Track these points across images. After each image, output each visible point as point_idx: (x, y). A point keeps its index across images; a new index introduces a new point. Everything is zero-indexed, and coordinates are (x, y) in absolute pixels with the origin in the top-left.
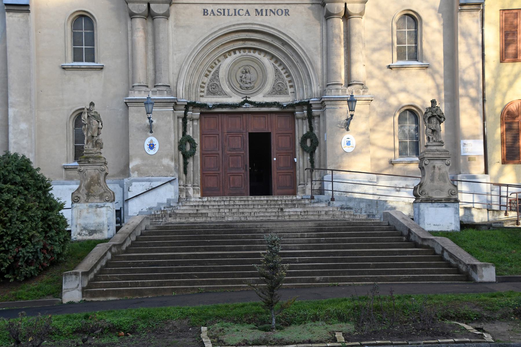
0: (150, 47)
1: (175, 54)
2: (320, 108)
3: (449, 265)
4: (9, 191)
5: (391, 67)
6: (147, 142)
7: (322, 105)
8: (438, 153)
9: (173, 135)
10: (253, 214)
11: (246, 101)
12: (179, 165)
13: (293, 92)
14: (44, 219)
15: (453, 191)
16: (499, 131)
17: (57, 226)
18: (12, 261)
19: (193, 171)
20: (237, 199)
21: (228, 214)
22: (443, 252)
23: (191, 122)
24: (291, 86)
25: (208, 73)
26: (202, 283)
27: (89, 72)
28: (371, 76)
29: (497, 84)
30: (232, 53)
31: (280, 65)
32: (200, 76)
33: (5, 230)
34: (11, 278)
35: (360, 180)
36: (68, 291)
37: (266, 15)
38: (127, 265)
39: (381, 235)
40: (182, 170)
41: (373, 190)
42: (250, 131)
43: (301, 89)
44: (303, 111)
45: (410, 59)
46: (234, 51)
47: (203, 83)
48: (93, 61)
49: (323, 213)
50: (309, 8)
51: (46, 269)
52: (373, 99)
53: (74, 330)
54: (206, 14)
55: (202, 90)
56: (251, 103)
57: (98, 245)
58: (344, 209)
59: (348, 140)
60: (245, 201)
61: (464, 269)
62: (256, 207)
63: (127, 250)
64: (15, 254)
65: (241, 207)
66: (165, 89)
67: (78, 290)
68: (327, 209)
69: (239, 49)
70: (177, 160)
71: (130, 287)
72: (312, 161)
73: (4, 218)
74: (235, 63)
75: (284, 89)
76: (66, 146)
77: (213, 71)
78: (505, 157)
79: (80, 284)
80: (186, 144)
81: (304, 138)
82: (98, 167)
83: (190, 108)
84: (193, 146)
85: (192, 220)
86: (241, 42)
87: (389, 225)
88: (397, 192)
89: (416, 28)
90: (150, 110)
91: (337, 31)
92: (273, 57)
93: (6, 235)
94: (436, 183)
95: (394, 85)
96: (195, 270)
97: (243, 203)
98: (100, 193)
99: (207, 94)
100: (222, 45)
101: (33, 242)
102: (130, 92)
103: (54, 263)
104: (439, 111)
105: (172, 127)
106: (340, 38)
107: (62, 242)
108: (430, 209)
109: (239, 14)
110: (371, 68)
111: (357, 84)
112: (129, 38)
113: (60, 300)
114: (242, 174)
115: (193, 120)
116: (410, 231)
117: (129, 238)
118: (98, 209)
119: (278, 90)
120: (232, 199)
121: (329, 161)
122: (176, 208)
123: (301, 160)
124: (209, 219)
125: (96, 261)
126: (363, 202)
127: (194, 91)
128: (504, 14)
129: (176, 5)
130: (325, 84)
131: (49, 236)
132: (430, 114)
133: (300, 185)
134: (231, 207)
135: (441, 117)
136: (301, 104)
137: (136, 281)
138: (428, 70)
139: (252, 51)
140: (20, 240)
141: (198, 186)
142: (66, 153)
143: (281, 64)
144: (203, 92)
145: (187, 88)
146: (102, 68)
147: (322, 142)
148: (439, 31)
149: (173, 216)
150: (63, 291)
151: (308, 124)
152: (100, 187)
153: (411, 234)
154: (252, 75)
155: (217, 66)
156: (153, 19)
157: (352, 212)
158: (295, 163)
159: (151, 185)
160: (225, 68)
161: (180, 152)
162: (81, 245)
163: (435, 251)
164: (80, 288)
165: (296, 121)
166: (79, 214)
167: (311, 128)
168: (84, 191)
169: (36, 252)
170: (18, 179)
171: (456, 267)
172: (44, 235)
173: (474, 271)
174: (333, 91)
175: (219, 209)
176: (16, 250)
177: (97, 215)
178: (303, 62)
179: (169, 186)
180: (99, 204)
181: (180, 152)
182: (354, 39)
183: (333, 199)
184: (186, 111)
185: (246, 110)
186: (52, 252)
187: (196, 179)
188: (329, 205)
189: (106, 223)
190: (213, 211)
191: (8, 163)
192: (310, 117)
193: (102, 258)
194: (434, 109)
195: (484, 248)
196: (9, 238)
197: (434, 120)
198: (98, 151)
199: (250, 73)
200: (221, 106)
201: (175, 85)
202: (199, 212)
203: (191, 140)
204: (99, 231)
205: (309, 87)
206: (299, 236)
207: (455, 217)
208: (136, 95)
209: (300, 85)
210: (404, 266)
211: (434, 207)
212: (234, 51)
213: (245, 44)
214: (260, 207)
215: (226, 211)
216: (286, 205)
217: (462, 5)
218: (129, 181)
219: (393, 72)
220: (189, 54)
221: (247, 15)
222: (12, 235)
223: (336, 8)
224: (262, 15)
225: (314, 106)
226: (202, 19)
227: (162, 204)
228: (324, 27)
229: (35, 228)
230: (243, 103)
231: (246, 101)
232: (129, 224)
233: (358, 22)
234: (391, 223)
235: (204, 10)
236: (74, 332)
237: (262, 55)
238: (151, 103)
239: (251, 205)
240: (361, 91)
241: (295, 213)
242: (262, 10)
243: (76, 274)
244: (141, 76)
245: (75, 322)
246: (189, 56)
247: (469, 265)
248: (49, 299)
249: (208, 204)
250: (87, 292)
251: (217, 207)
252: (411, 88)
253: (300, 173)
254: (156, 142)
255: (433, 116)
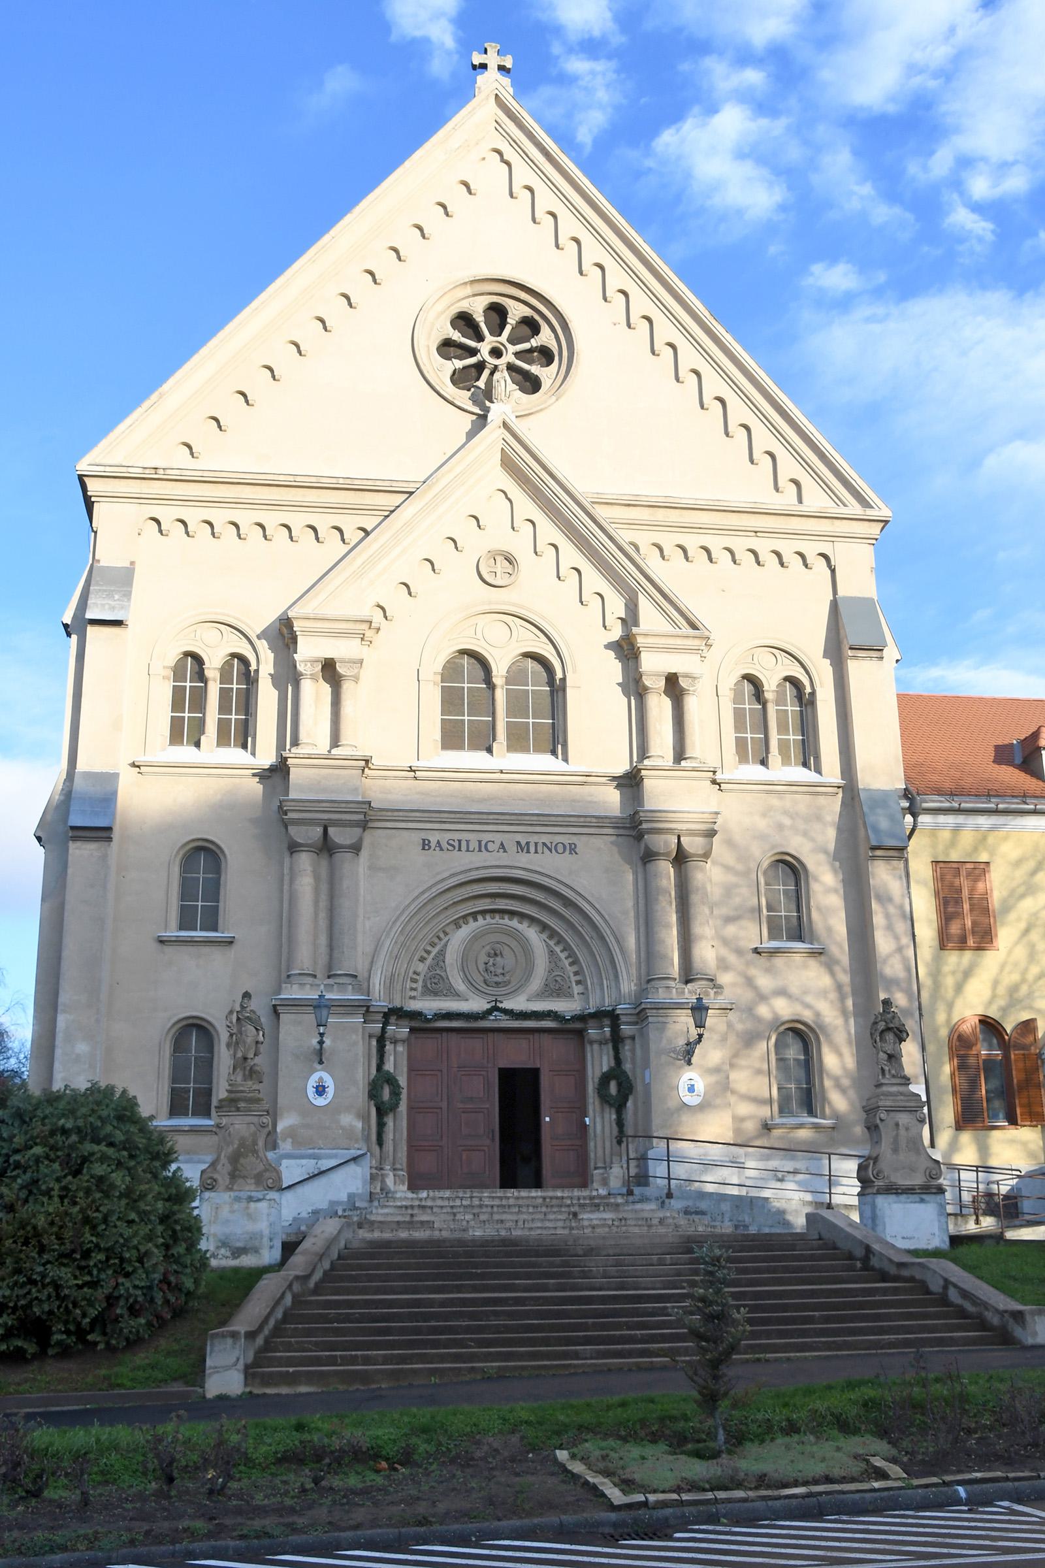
0: (323, 904)
1: (369, 918)
2: (636, 1023)
3: (962, 1313)
4: (104, 1158)
5: (760, 950)
6: (312, 1082)
7: (641, 1015)
8: (902, 1097)
9: (360, 1070)
10: (520, 1223)
11: (496, 1009)
12: (369, 1127)
13: (582, 994)
14: (164, 1219)
15: (934, 1172)
16: (947, 1069)
17: (190, 1235)
18: (104, 1305)
19: (394, 1140)
20: (486, 1195)
21: (472, 1223)
22: (945, 1288)
23: (392, 1046)
24: (578, 983)
25: (425, 955)
26: (488, 1357)
27: (205, 950)
28: (723, 965)
29: (937, 985)
30: (471, 920)
31: (558, 943)
32: (411, 960)
33: (94, 1239)
34: (99, 1342)
35: (715, 1158)
36: (218, 1372)
37: (536, 852)
38: (325, 1319)
39: (812, 1258)
40: (374, 1137)
41: (739, 1178)
42: (504, 1064)
43: (597, 987)
44: (602, 1027)
45: (791, 938)
46: (474, 915)
47: (415, 973)
48: (216, 930)
49: (655, 1222)
50: (612, 843)
51: (163, 1323)
52: (734, 1006)
53: (279, 1455)
54: (427, 847)
55: (414, 985)
56: (505, 1012)
57: (264, 1276)
58: (691, 1213)
59: (689, 1082)
60: (501, 1198)
61: (996, 1321)
62: (524, 1210)
63: (317, 1290)
64: (111, 1290)
65: (495, 1209)
66: (348, 982)
67: (238, 1370)
68: (661, 1214)
69: (484, 912)
70: (366, 1119)
71: (340, 1365)
72: (620, 1123)
73: (95, 1215)
74: (475, 938)
75: (566, 987)
76: (155, 1086)
77: (435, 951)
78: (961, 1119)
79: (242, 1357)
80: (382, 1088)
81: (605, 1079)
82: (255, 1120)
83: (393, 1019)
84: (396, 1093)
85: (403, 1235)
86: (488, 900)
87: (820, 1239)
88: (779, 1183)
89: (797, 883)
90: (324, 1019)
91: (664, 883)
92: (544, 927)
93: (96, 1250)
94: (902, 1156)
95: (765, 982)
96: (468, 1330)
97: (497, 1202)
98: (258, 1171)
99: (423, 994)
100: (454, 903)
101: (146, 1265)
102: (284, 985)
103: (179, 1313)
104: (897, 1019)
105: (361, 1054)
106: (670, 895)
107: (196, 1268)
108: (895, 1206)
109: (487, 850)
110: (724, 952)
111: (702, 979)
112: (286, 887)
113: (200, 1390)
114: (486, 1148)
115: (395, 1042)
116: (868, 1249)
117: (319, 1266)
118: (252, 1205)
119: (554, 989)
120: (474, 1195)
121: (656, 1121)
122: (370, 1210)
123: (598, 1120)
124: (437, 1233)
125: (268, 1310)
126: (725, 1200)
127: (399, 987)
128: (938, 870)
129: (372, 830)
130: (644, 979)
131: (173, 1255)
132: (882, 1026)
133: (596, 1168)
134: (476, 1211)
135: (901, 1031)
136: (599, 1015)
137: (353, 1353)
138: (823, 958)
139: (506, 917)
140: (122, 1260)
141: (402, 1170)
142: (155, 1101)
143: (560, 940)
144: (415, 989)
145: (388, 981)
146: (232, 942)
147: (639, 1088)
148: (836, 891)
149: (366, 1226)
150: (208, 1372)
151: (611, 1053)
152: (257, 1158)
153: (871, 1256)
154: (507, 960)
155: (443, 943)
156: (331, 855)
157: (706, 1220)
158: (585, 1126)
159: (319, 1165)
160: (457, 947)
161: (372, 1102)
162: (221, 1278)
163: (927, 1287)
164: (241, 1366)
165: (588, 1048)
166: (213, 1214)
167: (618, 1060)
168: (224, 1168)
169: (150, 1288)
170: (119, 1136)
171: (977, 1318)
172: (164, 1253)
173: (1018, 1324)
174: (660, 990)
175: (455, 1214)
176: (113, 1283)
177: (250, 1217)
178: (602, 938)
179: (352, 1168)
180: (253, 1194)
181: (372, 1102)
182: (695, 898)
183: (669, 1195)
184: (386, 1023)
185: (496, 1025)
186: (178, 1288)
187: (399, 1155)
188: (662, 1207)
189: (266, 1232)
190: (443, 1217)
191: (98, 1103)
192: (617, 1040)
193: (278, 1302)
194: (889, 1016)
195: (1015, 1279)
196: (101, 1257)
197: (890, 1037)
198: (255, 1087)
199: (502, 956)
200: (449, 1016)
201: (366, 975)
202: (416, 1219)
203: (391, 1080)
204: (251, 1248)
205: (613, 984)
206: (655, 1263)
207: (939, 1221)
208: (293, 992)
209: (595, 981)
210: (877, 1318)
211: (900, 1202)
212: (474, 915)
213: (493, 903)
214: (531, 1210)
215: (469, 1217)
216: (582, 1206)
217: (874, 848)
218: (275, 1156)
219: (762, 961)
220: (393, 919)
221: (501, 850)
222: (107, 1250)
223: (662, 844)
224: (528, 852)
225: (623, 1019)
226: (419, 857)
227: (338, 1203)
228: (640, 877)
229: (150, 1238)
230: (489, 1012)
231: (496, 1009)
232: (316, 1236)
233: (702, 870)
234: (825, 1235)
235: (424, 840)
236: (279, 1461)
237: (526, 924)
238: (326, 1006)
239: (515, 1205)
240: (712, 992)
241: (602, 1222)
242: (528, 843)
243: (234, 1335)
244: (306, 956)
245: (277, 1439)
246: (394, 922)
247: (1006, 1311)
248: (178, 1387)
249: (429, 1203)
250: (254, 1375)
251: (449, 1210)
252: (794, 989)
253: (595, 1147)
254: (329, 1082)
255: (888, 1029)
